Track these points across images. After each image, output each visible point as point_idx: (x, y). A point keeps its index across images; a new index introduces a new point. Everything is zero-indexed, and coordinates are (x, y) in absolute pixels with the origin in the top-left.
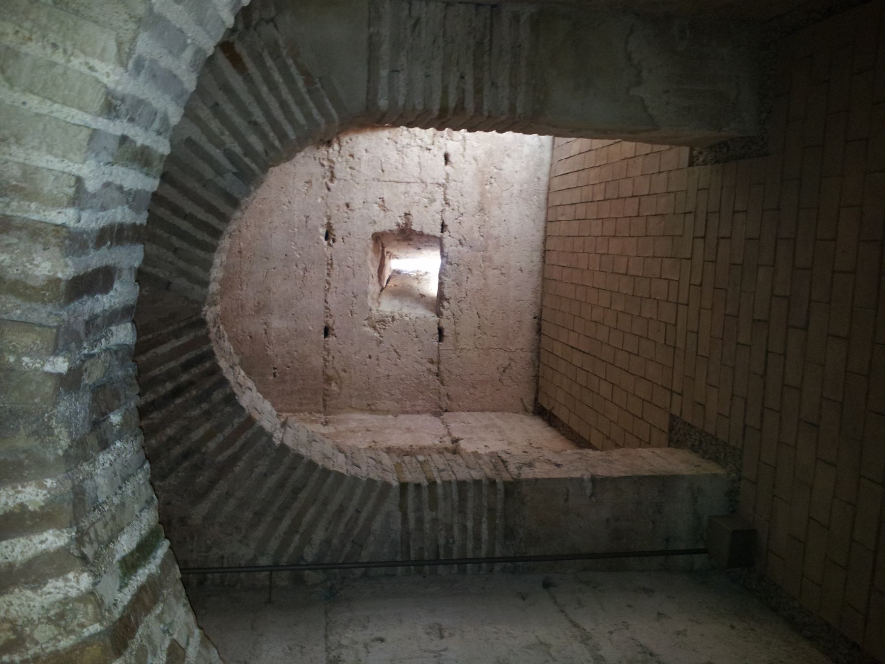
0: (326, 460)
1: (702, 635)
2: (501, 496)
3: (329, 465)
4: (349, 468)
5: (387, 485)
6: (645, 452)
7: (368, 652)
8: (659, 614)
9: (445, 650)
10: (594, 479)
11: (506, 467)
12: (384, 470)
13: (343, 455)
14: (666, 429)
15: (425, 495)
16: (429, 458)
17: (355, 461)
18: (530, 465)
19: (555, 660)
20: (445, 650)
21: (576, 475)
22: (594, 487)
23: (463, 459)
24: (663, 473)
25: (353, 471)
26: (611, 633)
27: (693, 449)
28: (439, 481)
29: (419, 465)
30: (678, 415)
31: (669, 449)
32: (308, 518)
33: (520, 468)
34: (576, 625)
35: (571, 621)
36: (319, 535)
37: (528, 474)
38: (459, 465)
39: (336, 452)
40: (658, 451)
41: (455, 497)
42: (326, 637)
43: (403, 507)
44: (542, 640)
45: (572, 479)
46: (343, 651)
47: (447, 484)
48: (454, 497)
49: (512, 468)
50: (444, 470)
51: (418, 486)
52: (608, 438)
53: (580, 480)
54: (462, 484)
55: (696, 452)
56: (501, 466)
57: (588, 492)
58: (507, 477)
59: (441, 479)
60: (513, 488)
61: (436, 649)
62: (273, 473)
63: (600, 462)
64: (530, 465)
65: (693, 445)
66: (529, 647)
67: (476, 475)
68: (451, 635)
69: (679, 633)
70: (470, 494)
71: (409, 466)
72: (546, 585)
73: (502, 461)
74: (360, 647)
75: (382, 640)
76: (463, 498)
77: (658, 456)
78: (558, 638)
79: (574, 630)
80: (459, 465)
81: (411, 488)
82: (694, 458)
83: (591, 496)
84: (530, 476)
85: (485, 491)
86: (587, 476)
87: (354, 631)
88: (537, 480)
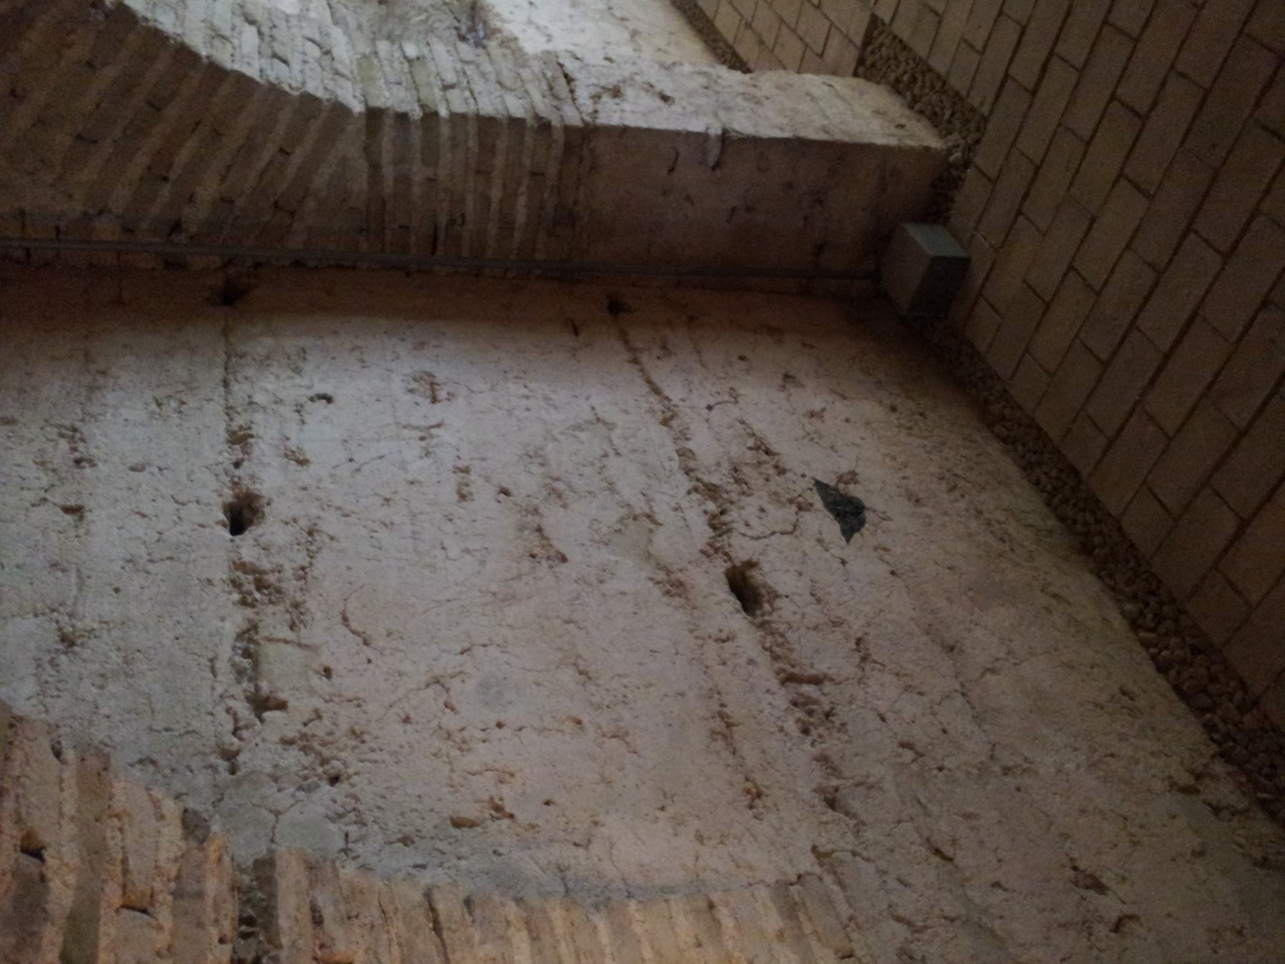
0: (217, 42)
1: (847, 421)
2: (557, 151)
3: (224, 57)
4: (265, 63)
5: (339, 110)
6: (813, 82)
7: (303, 422)
8: (787, 377)
9: (438, 426)
10: (726, 138)
11: (572, 91)
12: (337, 73)
13: (253, 30)
14: (858, 40)
15: (416, 137)
16: (426, 51)
17: (278, 49)
18: (616, 92)
19: (618, 454)
20: (438, 426)
21: (696, 126)
22: (723, 151)
23: (492, 62)
24: (847, 139)
25: (276, 72)
26: (710, 408)
27: (897, 88)
28: (443, 112)
29: (406, 65)
30: (887, 20)
31: (855, 81)
32: (183, 156)
33: (596, 98)
34: (656, 391)
35: (649, 382)
36: (208, 190)
37: (612, 114)
38: (483, 75)
39: (239, 21)
40: (838, 82)
41: (473, 144)
42: (226, 384)
43: (370, 151)
44: (600, 415)
45: (689, 135)
46: (258, 417)
47: (458, 119)
48: (471, 143)
49: (583, 95)
50: (452, 87)
51: (403, 118)
52: (749, 26)
53: (704, 137)
54: (487, 124)
55: (899, 93)
56: (561, 84)
57: (712, 160)
58: (573, 117)
59: (448, 108)
60: (584, 138)
61: (422, 423)
62: (105, 64)
63: (739, 100)
64: (616, 92)
65: (898, 80)
66: (579, 427)
67: (516, 107)
68: (451, 397)
69: (812, 415)
70: (502, 144)
71: (387, 69)
72: (615, 308)
73: (566, 76)
74: (287, 411)
75: (329, 399)
76: (487, 149)
77: (839, 96)
78: (626, 412)
79: (653, 398)
80: (483, 75)
81: (389, 121)
82: (894, 106)
83: (714, 168)
84: (615, 120)
85: (529, 139)
86: (716, 130)
87: (277, 377)
88: (625, 129)
